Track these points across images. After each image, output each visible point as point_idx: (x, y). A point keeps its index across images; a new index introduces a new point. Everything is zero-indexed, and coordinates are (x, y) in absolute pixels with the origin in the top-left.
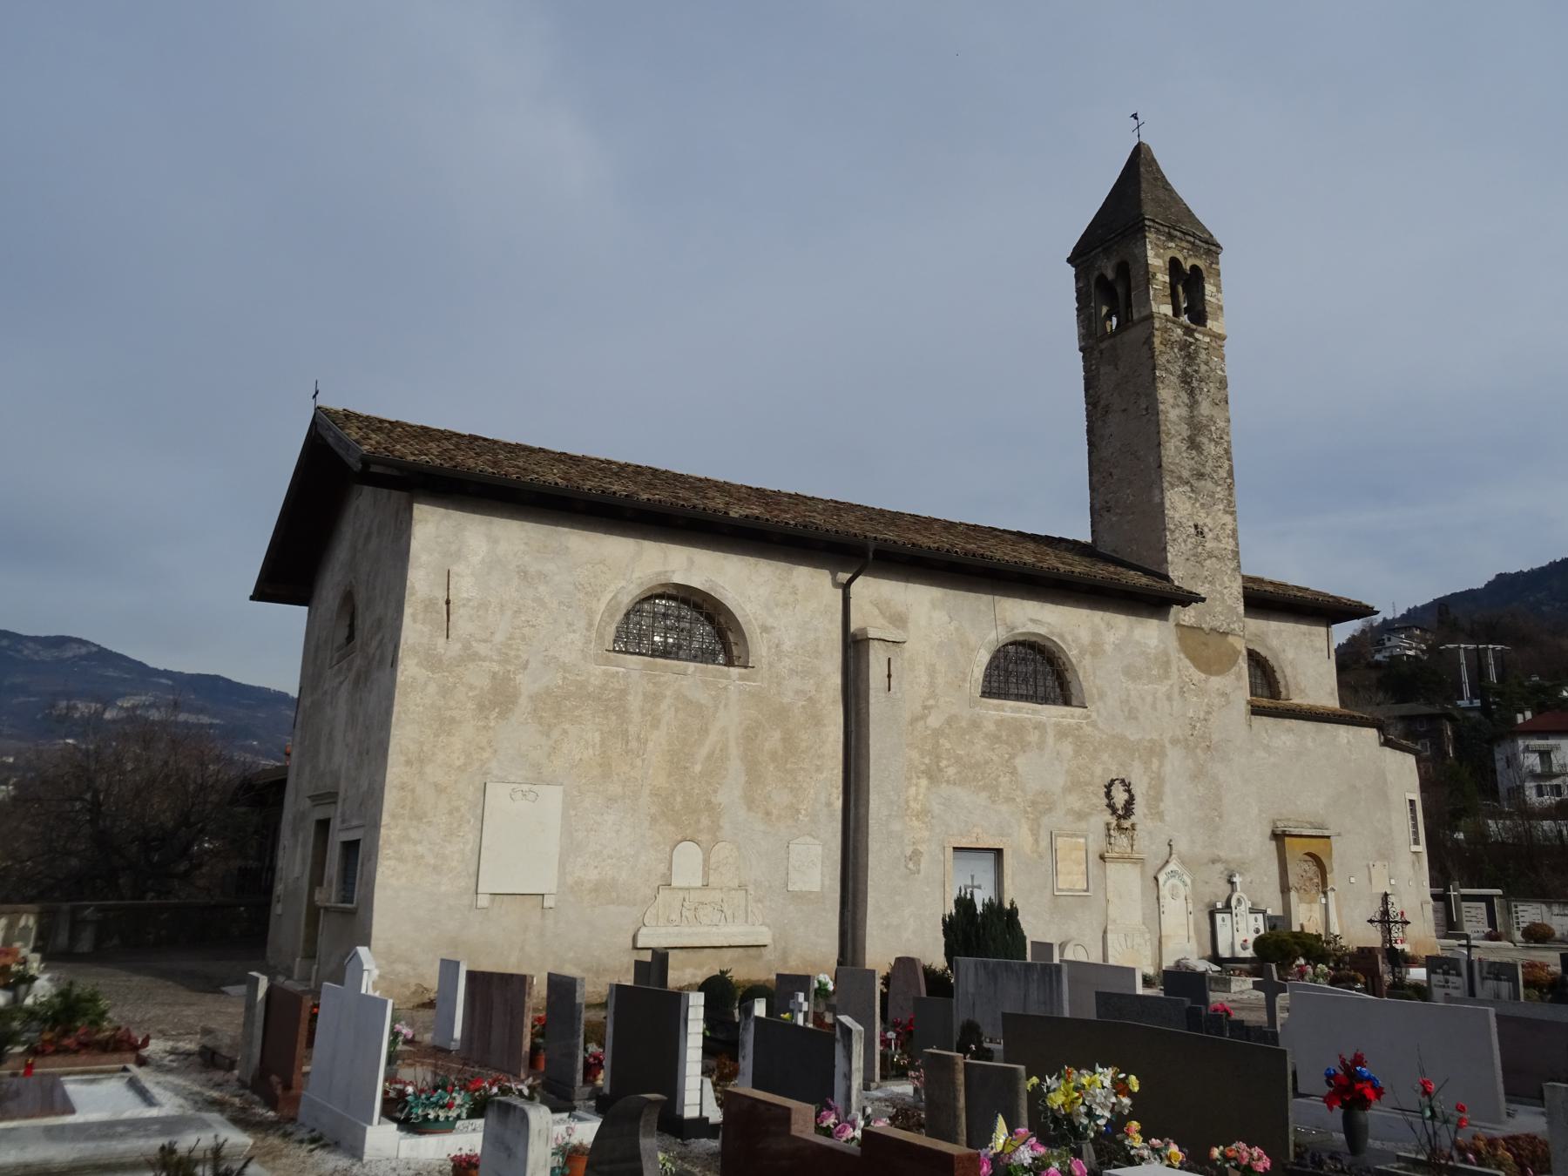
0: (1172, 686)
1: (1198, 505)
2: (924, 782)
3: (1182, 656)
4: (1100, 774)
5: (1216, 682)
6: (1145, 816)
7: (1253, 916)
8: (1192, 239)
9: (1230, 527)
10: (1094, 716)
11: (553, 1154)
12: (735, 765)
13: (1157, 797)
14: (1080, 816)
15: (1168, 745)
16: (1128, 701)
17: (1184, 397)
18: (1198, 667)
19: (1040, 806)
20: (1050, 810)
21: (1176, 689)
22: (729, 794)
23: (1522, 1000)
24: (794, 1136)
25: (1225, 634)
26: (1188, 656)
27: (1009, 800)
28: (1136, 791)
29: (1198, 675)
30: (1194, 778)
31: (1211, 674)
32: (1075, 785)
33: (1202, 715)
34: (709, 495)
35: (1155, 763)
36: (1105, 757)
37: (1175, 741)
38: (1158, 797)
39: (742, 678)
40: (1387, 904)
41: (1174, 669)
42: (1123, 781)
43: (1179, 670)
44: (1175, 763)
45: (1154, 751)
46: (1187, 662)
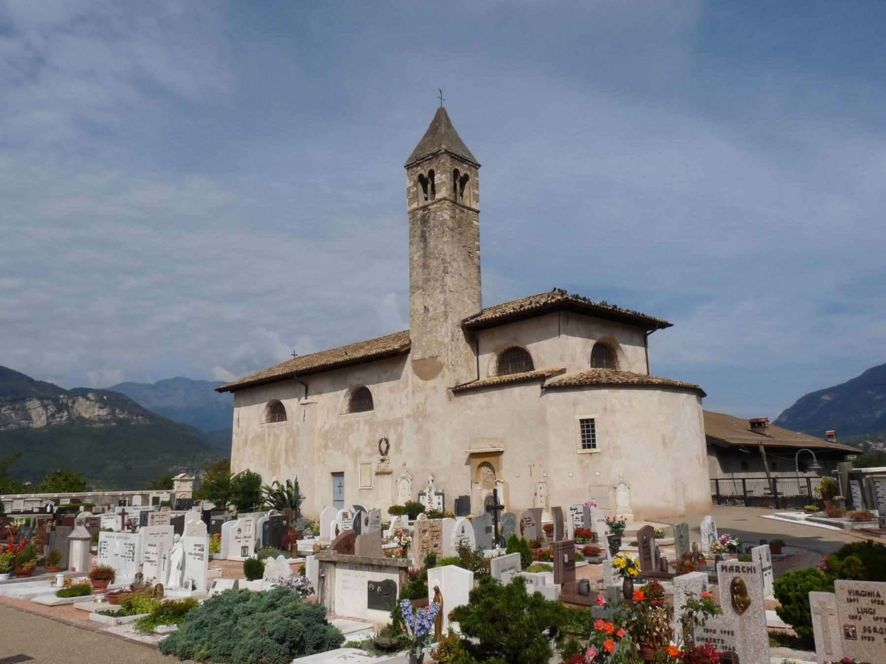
0: (408, 391)
1: (426, 296)
2: (323, 450)
3: (415, 375)
4: (378, 437)
5: (431, 383)
6: (394, 453)
7: (437, 497)
8: (427, 158)
9: (442, 299)
10: (376, 413)
11: (345, 397)
12: (283, 452)
13: (399, 443)
14: (370, 455)
15: (405, 419)
16: (389, 403)
17: (422, 245)
18: (421, 378)
19: (357, 453)
20: (360, 454)
21: (410, 392)
22: (282, 461)
23: (383, 546)
24: (386, 609)
25: (437, 357)
26: (417, 375)
27: (348, 452)
28: (391, 443)
29: (421, 382)
30: (418, 431)
31: (428, 380)
32: (369, 443)
33: (423, 401)
34: (255, 603)
35: (399, 429)
36: (380, 430)
37: (408, 416)
38: (400, 444)
39: (286, 424)
40: (754, 449)
41: (410, 383)
42: (385, 439)
43: (412, 383)
44: (409, 427)
45: (399, 423)
46: (417, 378)
